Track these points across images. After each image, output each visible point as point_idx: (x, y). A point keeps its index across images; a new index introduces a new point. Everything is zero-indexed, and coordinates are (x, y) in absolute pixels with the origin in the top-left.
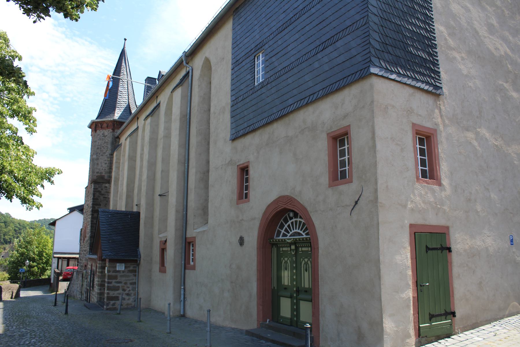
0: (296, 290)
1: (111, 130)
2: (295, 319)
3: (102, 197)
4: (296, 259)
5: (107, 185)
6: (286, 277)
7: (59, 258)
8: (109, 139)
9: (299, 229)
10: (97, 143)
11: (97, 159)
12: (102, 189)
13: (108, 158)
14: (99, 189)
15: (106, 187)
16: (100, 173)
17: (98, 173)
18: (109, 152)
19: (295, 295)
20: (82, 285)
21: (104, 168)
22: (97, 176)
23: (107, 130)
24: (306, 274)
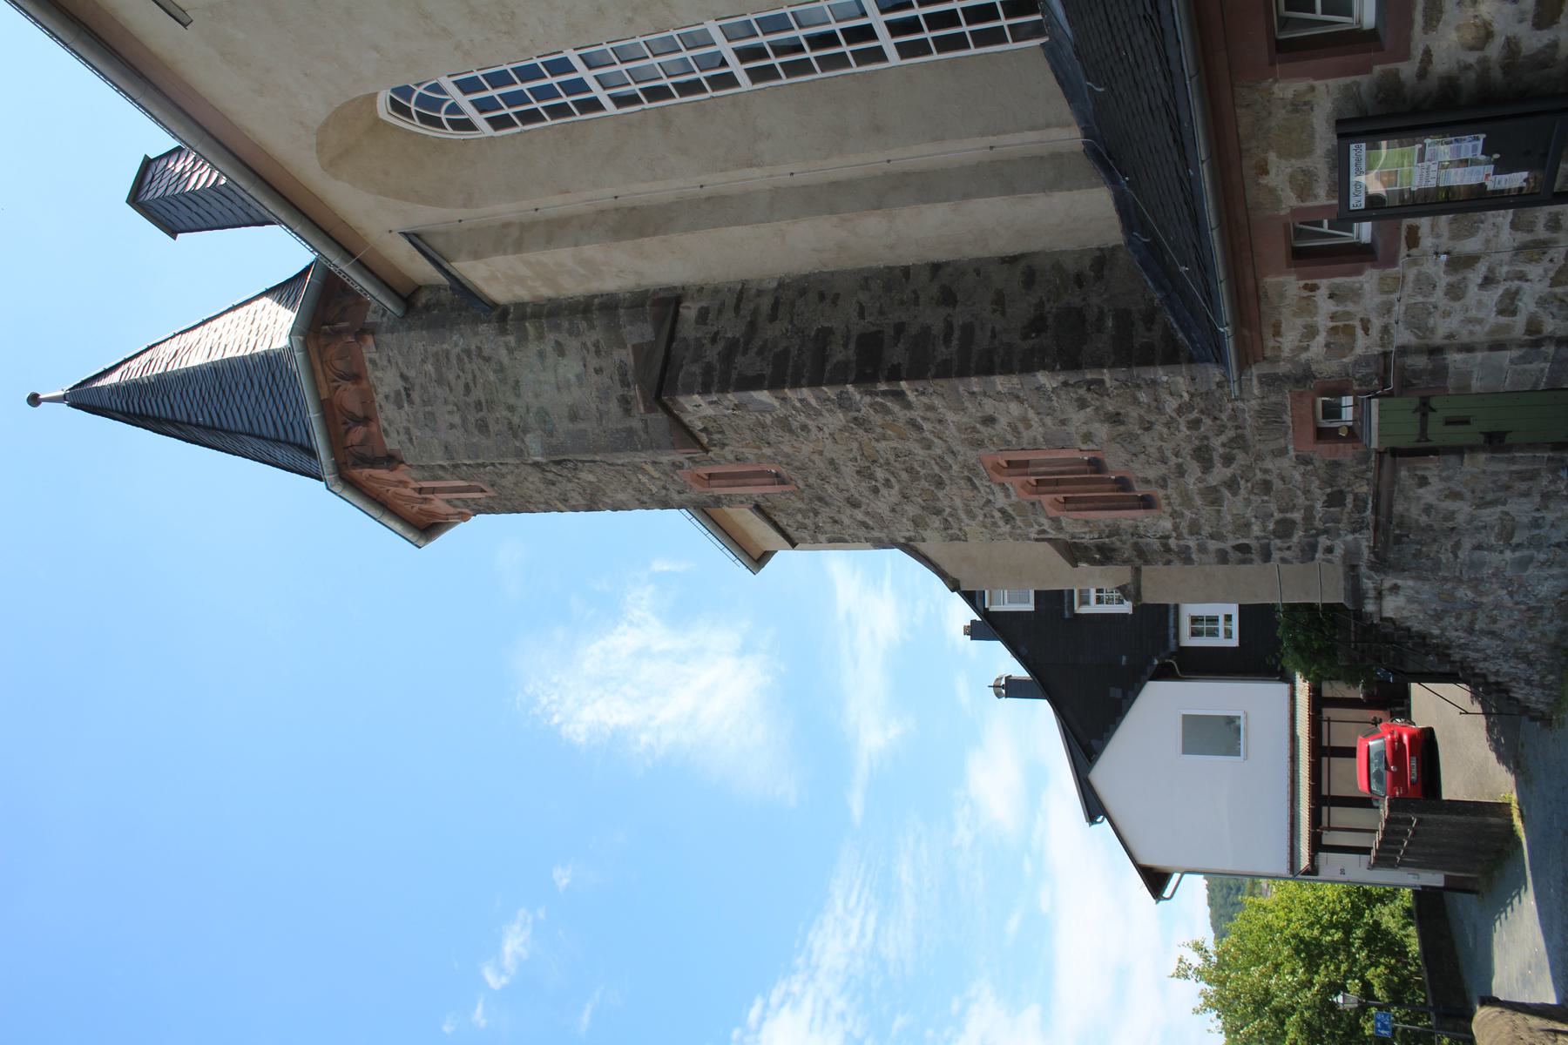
1: (369, 350)
3: (771, 331)
7: (1317, 846)
8: (418, 343)
12: (714, 339)
13: (523, 339)
14: (712, 353)
15: (703, 315)
16: (625, 383)
17: (625, 402)
18: (486, 337)
21: (594, 362)
23: (373, 375)
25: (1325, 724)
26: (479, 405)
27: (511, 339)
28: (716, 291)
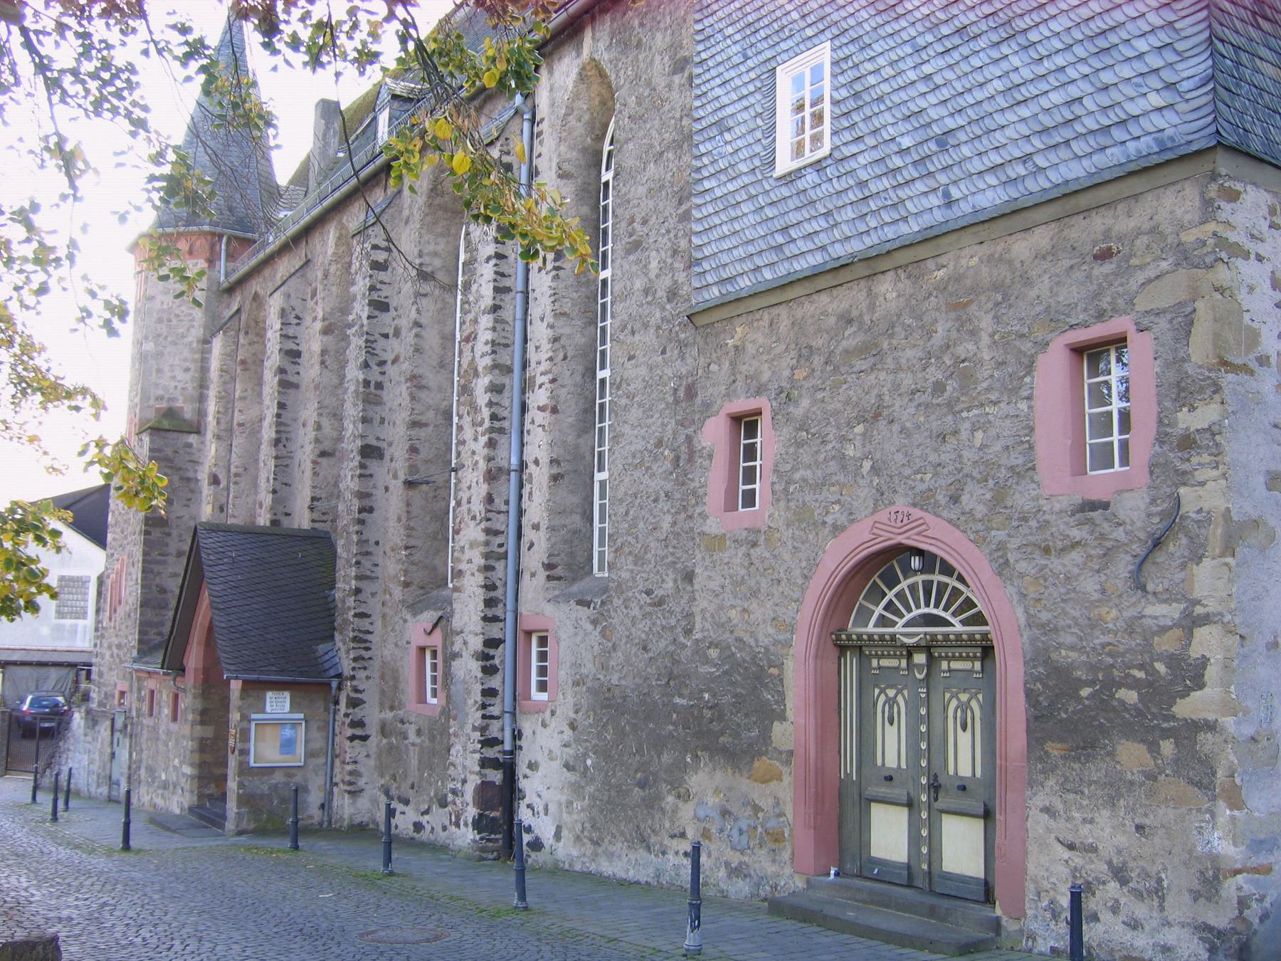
0: (930, 785)
2: (925, 867)
4: (928, 693)
5: (192, 439)
6: (892, 747)
9: (927, 605)
10: (157, 305)
11: (159, 355)
13: (193, 351)
14: (169, 452)
15: (190, 445)
16: (169, 399)
19: (924, 798)
20: (113, 755)
21: (180, 386)
22: (158, 410)
24: (964, 739)
25: (363, 175)
26: (169, 320)
27: (195, 345)
28: (200, 450)
